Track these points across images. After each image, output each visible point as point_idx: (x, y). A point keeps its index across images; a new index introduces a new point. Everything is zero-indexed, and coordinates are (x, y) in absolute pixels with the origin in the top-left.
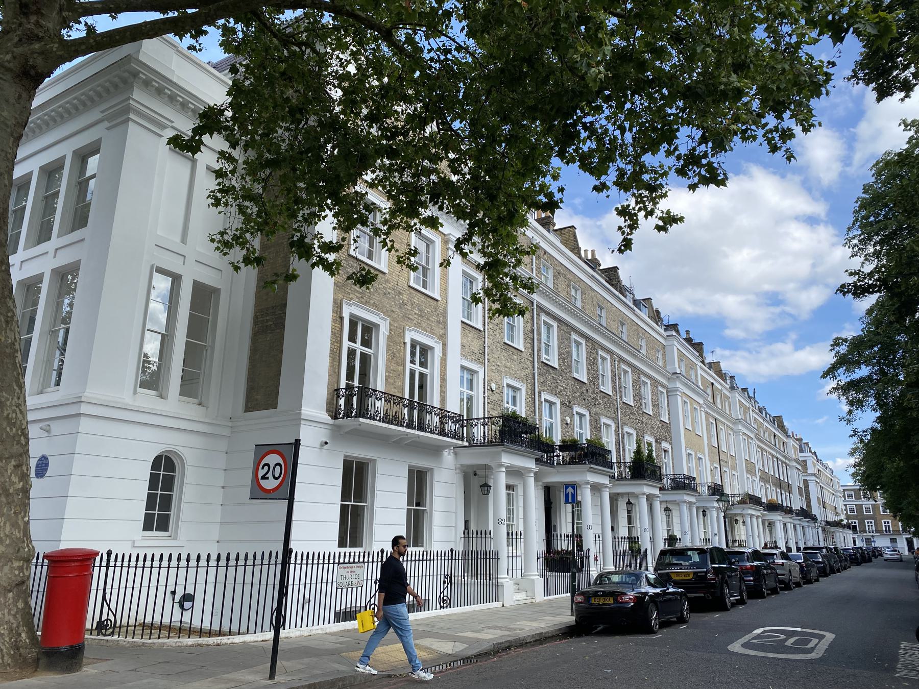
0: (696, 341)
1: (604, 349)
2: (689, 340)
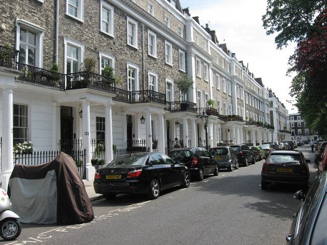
0: (211, 30)
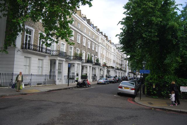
1: (85, 37)
2: (105, 35)
